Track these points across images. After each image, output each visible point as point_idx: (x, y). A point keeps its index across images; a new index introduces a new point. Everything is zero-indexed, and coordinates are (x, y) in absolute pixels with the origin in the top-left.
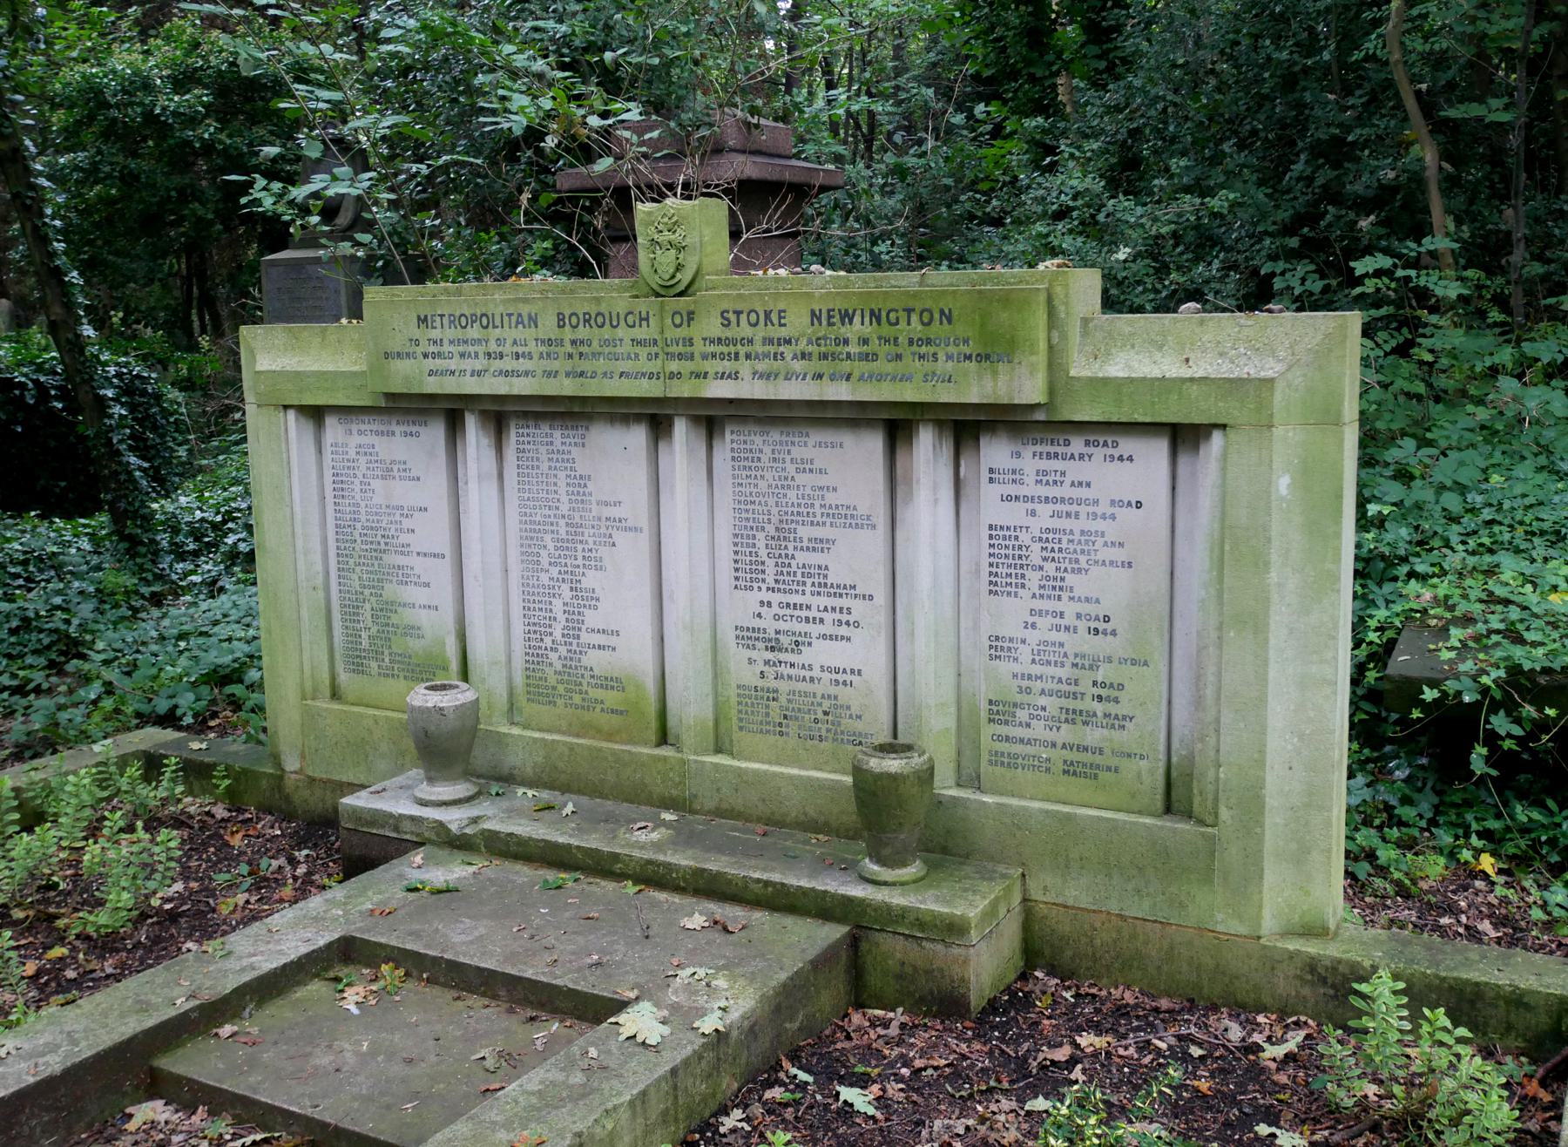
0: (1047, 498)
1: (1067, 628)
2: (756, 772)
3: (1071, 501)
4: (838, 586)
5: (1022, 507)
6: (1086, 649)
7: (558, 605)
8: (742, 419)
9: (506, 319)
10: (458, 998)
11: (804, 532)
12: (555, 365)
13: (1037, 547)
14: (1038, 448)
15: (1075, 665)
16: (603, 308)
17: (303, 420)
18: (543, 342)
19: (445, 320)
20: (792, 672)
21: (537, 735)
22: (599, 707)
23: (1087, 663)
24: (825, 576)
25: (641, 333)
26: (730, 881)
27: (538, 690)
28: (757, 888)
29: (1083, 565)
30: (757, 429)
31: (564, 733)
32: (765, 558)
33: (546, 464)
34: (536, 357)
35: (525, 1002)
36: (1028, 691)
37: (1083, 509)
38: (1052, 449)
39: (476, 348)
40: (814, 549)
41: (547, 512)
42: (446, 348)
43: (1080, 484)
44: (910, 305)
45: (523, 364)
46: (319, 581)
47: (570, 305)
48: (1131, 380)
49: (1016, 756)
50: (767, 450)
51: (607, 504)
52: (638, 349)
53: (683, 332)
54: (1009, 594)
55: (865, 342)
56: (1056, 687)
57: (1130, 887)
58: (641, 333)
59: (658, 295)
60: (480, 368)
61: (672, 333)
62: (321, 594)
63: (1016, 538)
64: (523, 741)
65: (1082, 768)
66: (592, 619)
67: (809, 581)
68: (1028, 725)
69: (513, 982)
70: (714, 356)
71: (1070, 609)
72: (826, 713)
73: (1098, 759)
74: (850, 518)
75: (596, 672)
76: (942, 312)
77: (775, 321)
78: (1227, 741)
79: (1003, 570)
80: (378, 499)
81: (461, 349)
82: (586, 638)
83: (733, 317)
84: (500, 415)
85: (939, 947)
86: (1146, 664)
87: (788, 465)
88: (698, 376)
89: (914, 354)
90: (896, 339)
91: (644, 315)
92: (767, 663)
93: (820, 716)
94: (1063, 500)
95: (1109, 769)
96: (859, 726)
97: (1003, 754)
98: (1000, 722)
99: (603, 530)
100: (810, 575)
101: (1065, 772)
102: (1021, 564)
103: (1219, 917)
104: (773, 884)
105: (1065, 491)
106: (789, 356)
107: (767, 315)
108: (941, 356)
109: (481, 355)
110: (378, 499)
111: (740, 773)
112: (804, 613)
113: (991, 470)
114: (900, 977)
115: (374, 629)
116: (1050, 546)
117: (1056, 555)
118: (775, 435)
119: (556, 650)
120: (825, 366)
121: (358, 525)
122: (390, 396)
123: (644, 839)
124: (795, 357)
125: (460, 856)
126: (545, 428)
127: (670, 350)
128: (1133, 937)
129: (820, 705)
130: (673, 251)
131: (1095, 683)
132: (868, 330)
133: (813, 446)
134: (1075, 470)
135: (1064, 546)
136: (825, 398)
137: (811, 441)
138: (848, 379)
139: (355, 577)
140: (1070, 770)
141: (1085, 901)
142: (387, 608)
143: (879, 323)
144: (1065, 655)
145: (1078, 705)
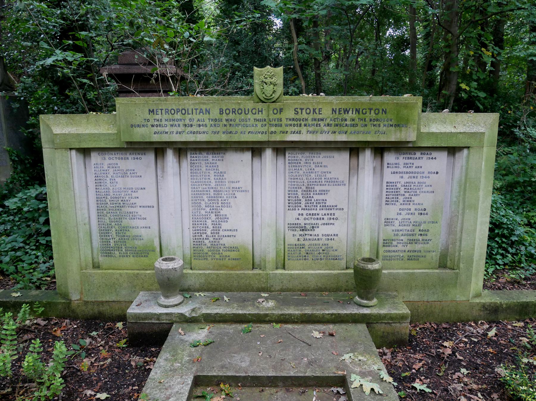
0: (407, 172)
1: (412, 214)
2: (298, 275)
3: (415, 173)
4: (330, 206)
5: (398, 175)
6: (418, 220)
7: (209, 222)
8: (294, 149)
9: (194, 111)
10: (263, 390)
11: (317, 188)
12: (218, 129)
13: (403, 188)
14: (405, 156)
15: (414, 225)
16: (242, 107)
17: (78, 154)
18: (212, 120)
19: (163, 112)
20: (311, 237)
21: (201, 272)
22: (227, 258)
23: (417, 224)
24: (325, 203)
25: (259, 116)
26: (317, 316)
27: (198, 252)
28: (327, 317)
29: (418, 193)
30: (300, 152)
31: (211, 270)
32: (301, 198)
33: (205, 168)
34: (208, 126)
36: (397, 235)
37: (419, 175)
38: (409, 156)
39: (179, 122)
40: (321, 194)
41: (205, 187)
42: (164, 122)
43: (418, 167)
44: (371, 107)
45: (202, 129)
46: (87, 221)
47: (226, 105)
48: (441, 133)
49: (392, 256)
50: (304, 159)
51: (233, 182)
52: (257, 123)
53: (278, 116)
54: (392, 204)
55: (353, 120)
56: (406, 233)
57: (431, 292)
58: (259, 116)
59: (263, 102)
60: (181, 130)
61: (272, 116)
62: (88, 226)
63: (396, 186)
64: (194, 276)
65: (414, 257)
66: (224, 226)
67: (319, 205)
68: (397, 246)
69: (285, 379)
70: (291, 125)
71: (413, 207)
72: (323, 250)
73: (419, 254)
74: (336, 182)
75: (226, 246)
76: (383, 110)
77: (317, 112)
78: (464, 243)
79: (391, 197)
81: (171, 123)
82: (221, 233)
83: (300, 111)
84: (182, 149)
85: (398, 325)
86: (437, 222)
87: (312, 164)
88: (283, 133)
89: (371, 124)
90: (365, 119)
91: (260, 109)
92: (301, 235)
93: (321, 251)
94: (412, 173)
95: (423, 256)
96: (336, 253)
97: (387, 256)
98: (387, 246)
99: (231, 192)
100: (319, 203)
101: (408, 259)
102: (397, 194)
103: (458, 296)
104: (335, 314)
105: (413, 170)
106: (322, 125)
107: (314, 110)
108: (382, 125)
109: (181, 125)
111: (291, 275)
112: (316, 217)
113: (388, 164)
114: (382, 337)
115: (117, 239)
116: (407, 188)
117: (409, 191)
118: (307, 154)
119: (208, 239)
120: (336, 129)
121: (109, 197)
122: (128, 143)
123: (268, 305)
124: (325, 125)
125: (196, 326)
126: (205, 154)
127: (271, 123)
128: (431, 307)
129: (321, 248)
130: (272, 86)
131: (420, 230)
132: (354, 116)
133: (322, 158)
134: (417, 163)
135: (412, 187)
136: (336, 140)
137: (321, 156)
138: (346, 133)
140: (410, 259)
141: (416, 299)
142: (123, 230)
143: (359, 113)
144: (411, 222)
145: (414, 238)
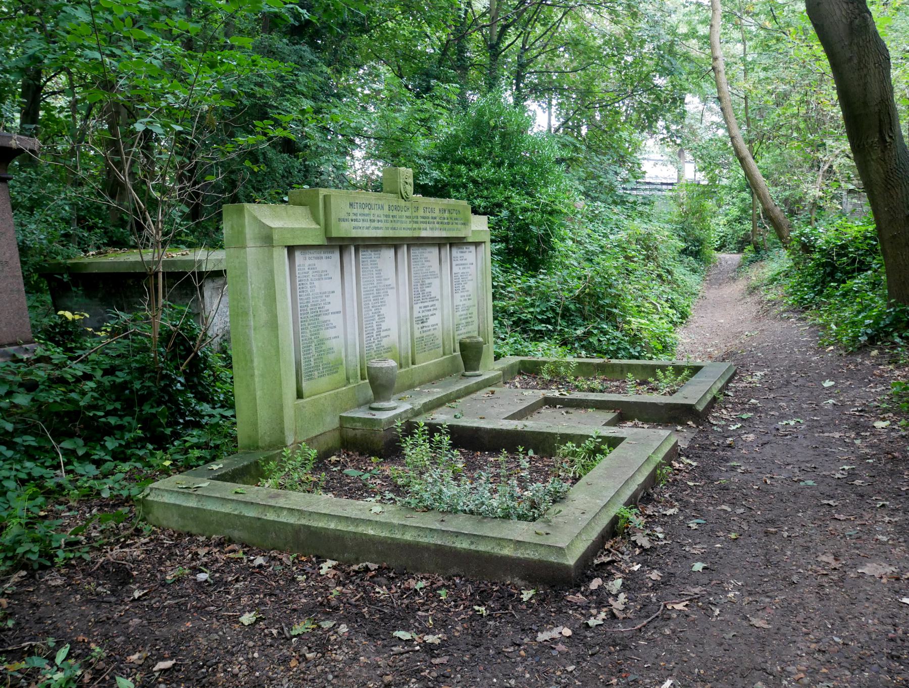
35: (533, 411)
42: (359, 217)
80: (317, 290)
110: (317, 290)
139: (308, 331)
